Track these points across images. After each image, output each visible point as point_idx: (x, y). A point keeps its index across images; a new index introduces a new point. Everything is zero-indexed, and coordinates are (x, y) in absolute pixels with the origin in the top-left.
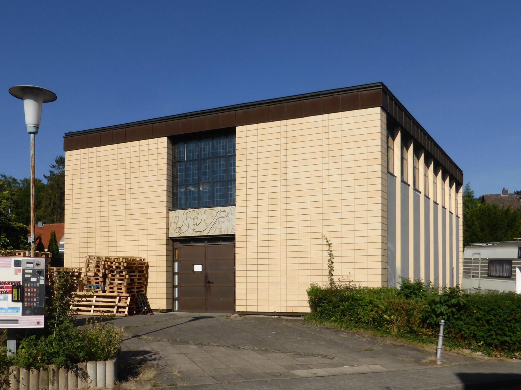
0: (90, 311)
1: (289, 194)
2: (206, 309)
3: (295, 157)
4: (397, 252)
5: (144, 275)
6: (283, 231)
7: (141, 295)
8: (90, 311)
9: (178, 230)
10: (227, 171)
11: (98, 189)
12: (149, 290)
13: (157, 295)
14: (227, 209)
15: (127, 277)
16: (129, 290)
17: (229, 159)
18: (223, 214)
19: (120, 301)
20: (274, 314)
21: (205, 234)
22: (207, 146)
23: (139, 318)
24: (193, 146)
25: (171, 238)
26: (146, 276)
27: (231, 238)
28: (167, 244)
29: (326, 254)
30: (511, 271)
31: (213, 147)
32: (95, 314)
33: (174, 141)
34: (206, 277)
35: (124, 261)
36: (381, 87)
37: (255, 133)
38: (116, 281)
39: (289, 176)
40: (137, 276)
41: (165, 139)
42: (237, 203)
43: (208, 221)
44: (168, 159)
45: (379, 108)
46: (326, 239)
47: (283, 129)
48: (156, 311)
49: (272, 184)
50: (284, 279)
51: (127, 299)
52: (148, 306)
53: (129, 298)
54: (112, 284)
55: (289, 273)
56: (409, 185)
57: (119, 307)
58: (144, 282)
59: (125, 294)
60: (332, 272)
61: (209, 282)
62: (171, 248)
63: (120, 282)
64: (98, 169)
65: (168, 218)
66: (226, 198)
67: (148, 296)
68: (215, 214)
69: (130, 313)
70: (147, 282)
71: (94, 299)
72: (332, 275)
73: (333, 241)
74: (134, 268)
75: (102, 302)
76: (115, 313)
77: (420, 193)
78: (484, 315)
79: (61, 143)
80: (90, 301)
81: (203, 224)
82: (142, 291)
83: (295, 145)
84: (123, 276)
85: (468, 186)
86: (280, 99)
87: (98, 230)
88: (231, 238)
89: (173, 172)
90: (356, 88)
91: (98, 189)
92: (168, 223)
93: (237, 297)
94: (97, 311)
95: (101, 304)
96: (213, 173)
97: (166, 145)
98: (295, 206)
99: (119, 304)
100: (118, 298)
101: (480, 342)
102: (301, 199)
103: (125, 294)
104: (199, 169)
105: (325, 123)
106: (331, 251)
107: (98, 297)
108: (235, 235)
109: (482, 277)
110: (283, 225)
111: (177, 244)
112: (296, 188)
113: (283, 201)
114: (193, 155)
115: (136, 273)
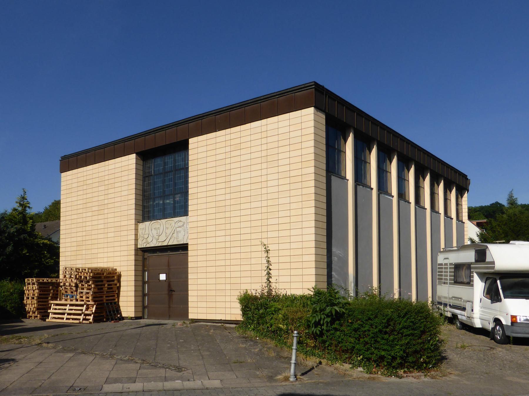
0: (63, 319)
1: (233, 202)
2: (169, 316)
3: (238, 165)
4: (349, 258)
5: (116, 285)
6: (228, 238)
7: (111, 303)
8: (63, 319)
9: (144, 241)
11: (85, 206)
12: (121, 299)
13: (127, 305)
14: (183, 219)
15: (93, 286)
17: (183, 170)
18: (180, 224)
19: (87, 309)
20: (220, 321)
21: (165, 244)
22: (169, 160)
23: (109, 326)
24: (159, 161)
25: (140, 248)
26: (118, 285)
27: (184, 247)
28: (136, 255)
29: (264, 261)
30: (454, 276)
31: (175, 160)
33: (144, 156)
34: (169, 286)
35: (90, 271)
36: (314, 86)
37: (204, 143)
38: (85, 291)
39: (233, 184)
40: (106, 285)
41: (134, 156)
42: (190, 213)
43: (168, 231)
44: (136, 174)
45: (312, 109)
47: (228, 137)
48: (126, 318)
49: (218, 192)
50: (228, 287)
51: (93, 307)
52: (121, 314)
53: (95, 306)
54: (82, 293)
55: (233, 281)
56: (372, 189)
57: (86, 315)
58: (116, 291)
59: (91, 303)
60: (270, 279)
61: (171, 290)
62: (140, 258)
63: (88, 291)
64: (85, 187)
65: (136, 230)
66: (181, 209)
67: (121, 304)
68: (173, 224)
69: (96, 320)
70: (119, 291)
71: (68, 307)
72: (270, 282)
73: (271, 247)
74: (103, 277)
75: (75, 310)
76: (81, 321)
77: (393, 197)
78: (362, 325)
81: (164, 234)
82: (114, 299)
83: (238, 153)
84: (90, 285)
85: (512, 194)
86: (225, 109)
87: (84, 243)
88: (184, 247)
89: (143, 186)
90: (291, 90)
91: (85, 206)
92: (136, 235)
93: (190, 304)
95: (73, 312)
96: (175, 184)
97: (134, 161)
98: (238, 213)
99: (87, 312)
100: (85, 306)
101: (360, 357)
102: (243, 206)
104: (164, 182)
105: (264, 129)
106: (269, 258)
107: (71, 305)
108: (187, 244)
109: (450, 284)
110: (228, 232)
111: (147, 255)
112: (238, 195)
113: (228, 209)
114: (159, 170)
115: (104, 282)
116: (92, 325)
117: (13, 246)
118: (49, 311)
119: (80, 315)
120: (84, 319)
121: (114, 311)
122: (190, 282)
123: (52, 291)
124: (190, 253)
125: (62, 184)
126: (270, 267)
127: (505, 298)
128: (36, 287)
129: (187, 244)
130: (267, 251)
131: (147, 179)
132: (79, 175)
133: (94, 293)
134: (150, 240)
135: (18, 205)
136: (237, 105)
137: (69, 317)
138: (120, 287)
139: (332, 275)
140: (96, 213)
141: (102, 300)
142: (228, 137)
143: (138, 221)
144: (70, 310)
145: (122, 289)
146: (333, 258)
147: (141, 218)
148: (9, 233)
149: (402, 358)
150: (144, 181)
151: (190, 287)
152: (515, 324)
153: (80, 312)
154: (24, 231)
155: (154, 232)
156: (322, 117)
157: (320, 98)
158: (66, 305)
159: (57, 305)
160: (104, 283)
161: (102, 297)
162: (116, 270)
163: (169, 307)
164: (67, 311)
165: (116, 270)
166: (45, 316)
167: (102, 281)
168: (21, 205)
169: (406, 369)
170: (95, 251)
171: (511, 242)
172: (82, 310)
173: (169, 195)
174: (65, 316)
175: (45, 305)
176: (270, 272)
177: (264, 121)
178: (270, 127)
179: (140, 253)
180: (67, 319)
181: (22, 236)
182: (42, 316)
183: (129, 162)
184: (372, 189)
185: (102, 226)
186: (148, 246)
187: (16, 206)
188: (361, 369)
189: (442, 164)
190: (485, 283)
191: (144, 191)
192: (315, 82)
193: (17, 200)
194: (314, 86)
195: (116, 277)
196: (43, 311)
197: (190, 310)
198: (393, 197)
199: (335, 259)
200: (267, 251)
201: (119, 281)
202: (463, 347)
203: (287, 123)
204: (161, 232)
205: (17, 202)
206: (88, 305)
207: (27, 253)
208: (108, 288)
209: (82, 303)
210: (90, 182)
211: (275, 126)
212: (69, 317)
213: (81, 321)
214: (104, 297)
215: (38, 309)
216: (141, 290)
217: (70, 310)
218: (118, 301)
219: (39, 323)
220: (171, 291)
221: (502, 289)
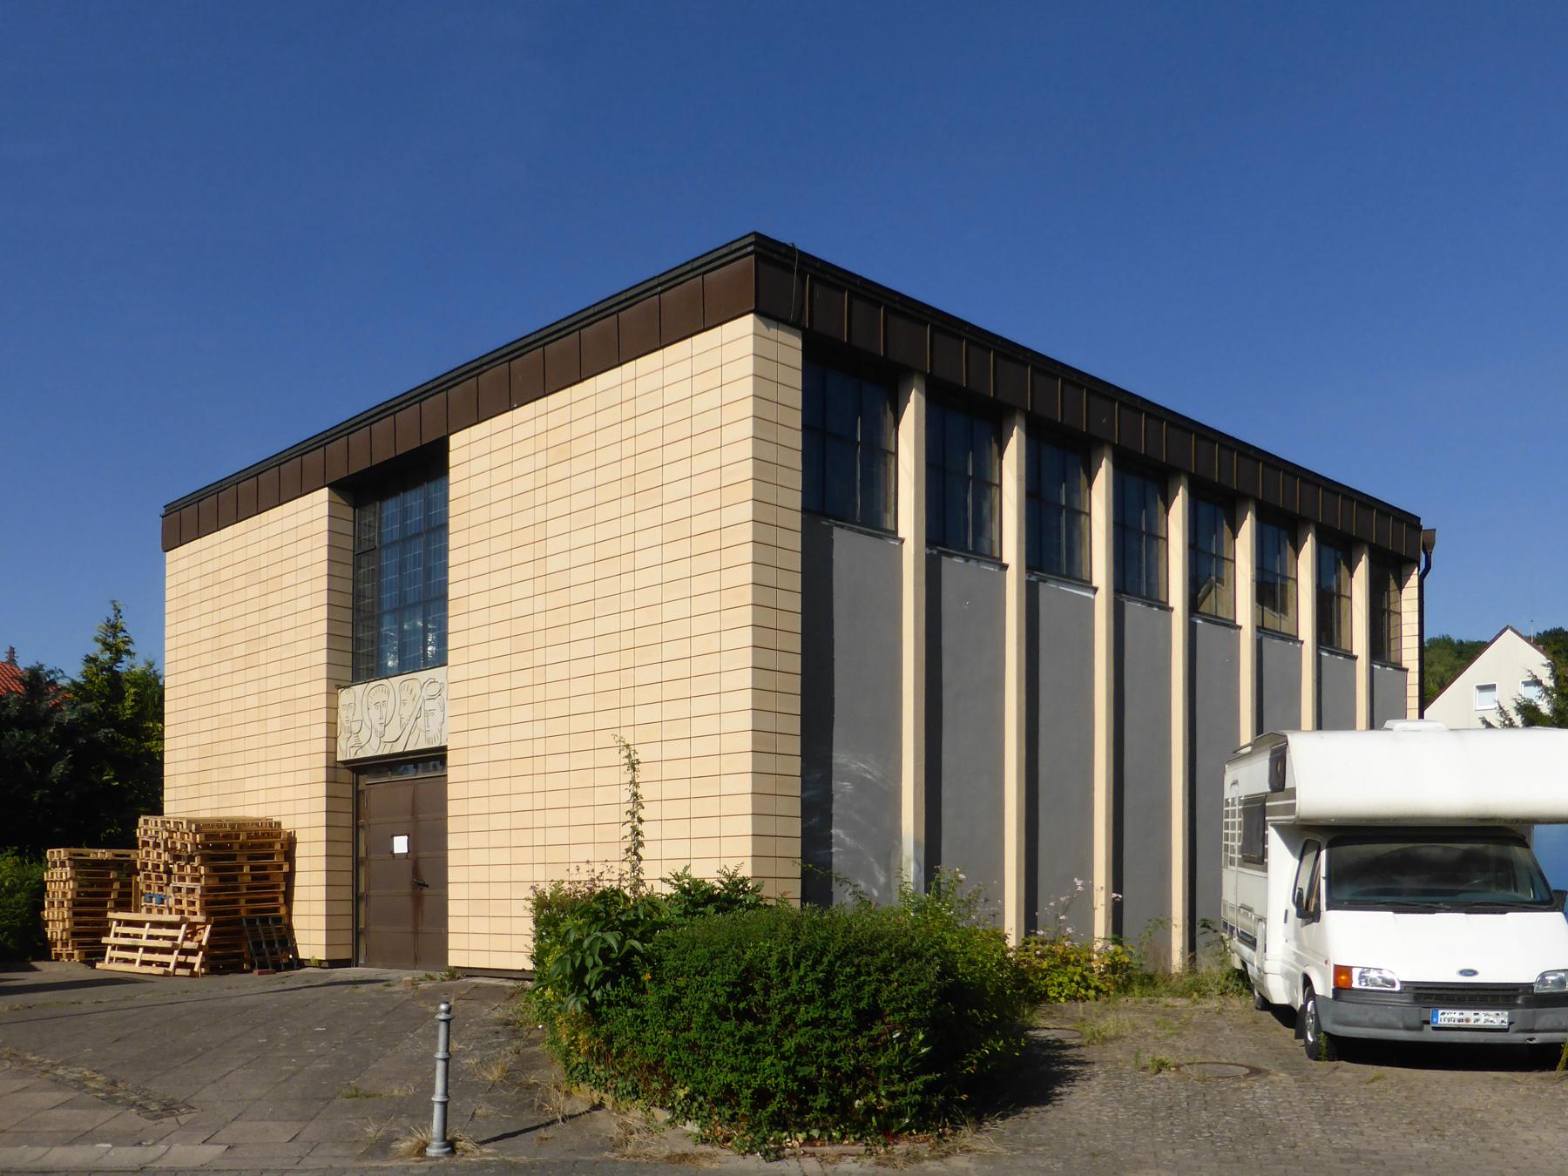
5: (280, 867)
7: (264, 921)
10: (428, 573)
12: (297, 908)
16: (210, 907)
17: (436, 529)
18: (433, 689)
21: (398, 748)
23: (250, 986)
25: (345, 762)
26: (286, 868)
27: (436, 758)
28: (330, 781)
29: (627, 796)
32: (146, 969)
34: (416, 870)
36: (750, 249)
39: (553, 564)
40: (246, 869)
42: (452, 657)
43: (407, 711)
46: (628, 746)
47: (541, 425)
52: (295, 952)
54: (180, 889)
56: (1005, 567)
57: (184, 952)
58: (278, 886)
59: (199, 918)
60: (641, 851)
62: (347, 791)
63: (192, 885)
65: (332, 708)
67: (297, 923)
68: (417, 690)
71: (145, 931)
73: (642, 754)
74: (236, 847)
76: (171, 969)
79: (155, 527)
80: (137, 936)
82: (277, 910)
88: (436, 758)
93: (452, 925)
94: (149, 963)
97: (324, 509)
99: (188, 945)
103: (199, 918)
106: (637, 785)
108: (444, 749)
111: (365, 780)
115: (240, 860)
116: (200, 980)
117: (71, 761)
118: (104, 940)
119: (169, 951)
120: (179, 965)
121: (270, 944)
122: (452, 858)
123: (116, 885)
124: (452, 774)
125: (169, 582)
126: (642, 814)
127: (1329, 908)
128: (67, 872)
129: (444, 749)
130: (633, 766)
131: (364, 559)
132: (205, 556)
133: (207, 890)
134: (364, 737)
135: (99, 646)
136: (561, 326)
137: (148, 957)
138: (292, 872)
139: (831, 836)
140: (240, 664)
141: (237, 912)
142: (541, 425)
143: (336, 685)
144: (154, 935)
145: (299, 879)
146: (837, 784)
147: (347, 674)
148: (59, 725)
149: (790, 1096)
150: (356, 566)
151: (452, 875)
152: (1344, 995)
153: (167, 944)
154: (113, 720)
155: (375, 714)
156: (790, 347)
157: (781, 282)
158: (141, 924)
159: (129, 923)
160: (243, 867)
161: (235, 902)
162: (278, 824)
163: (416, 933)
164: (144, 942)
165: (278, 824)
166: (94, 954)
167: (233, 857)
168: (108, 647)
169: (815, 1133)
170: (238, 772)
171: (1388, 724)
172: (175, 938)
173: (414, 605)
174: (139, 956)
175: (99, 924)
176: (640, 828)
177: (628, 368)
178: (643, 385)
179: (346, 775)
180: (143, 963)
181: (101, 733)
182: (87, 955)
183: (312, 511)
184: (1005, 567)
185: (252, 701)
186: (361, 755)
187: (95, 649)
188: (692, 1127)
189: (1304, 481)
190: (1301, 859)
191: (357, 595)
192: (756, 234)
193: (97, 634)
194: (750, 249)
195: (278, 847)
196: (88, 939)
197: (452, 941)
198: (1095, 590)
199: (842, 787)
200: (633, 766)
201: (290, 856)
202: (1161, 1066)
203: (684, 370)
204: (385, 716)
205: (97, 640)
206: (192, 925)
207: (115, 779)
208: (254, 878)
209: (176, 918)
210: (226, 574)
211: (655, 381)
212: (148, 957)
213: (171, 969)
214: (242, 902)
215: (74, 934)
216: (349, 881)
217: (154, 935)
218: (289, 914)
219: (83, 973)
220: (419, 885)
221: (1328, 878)
